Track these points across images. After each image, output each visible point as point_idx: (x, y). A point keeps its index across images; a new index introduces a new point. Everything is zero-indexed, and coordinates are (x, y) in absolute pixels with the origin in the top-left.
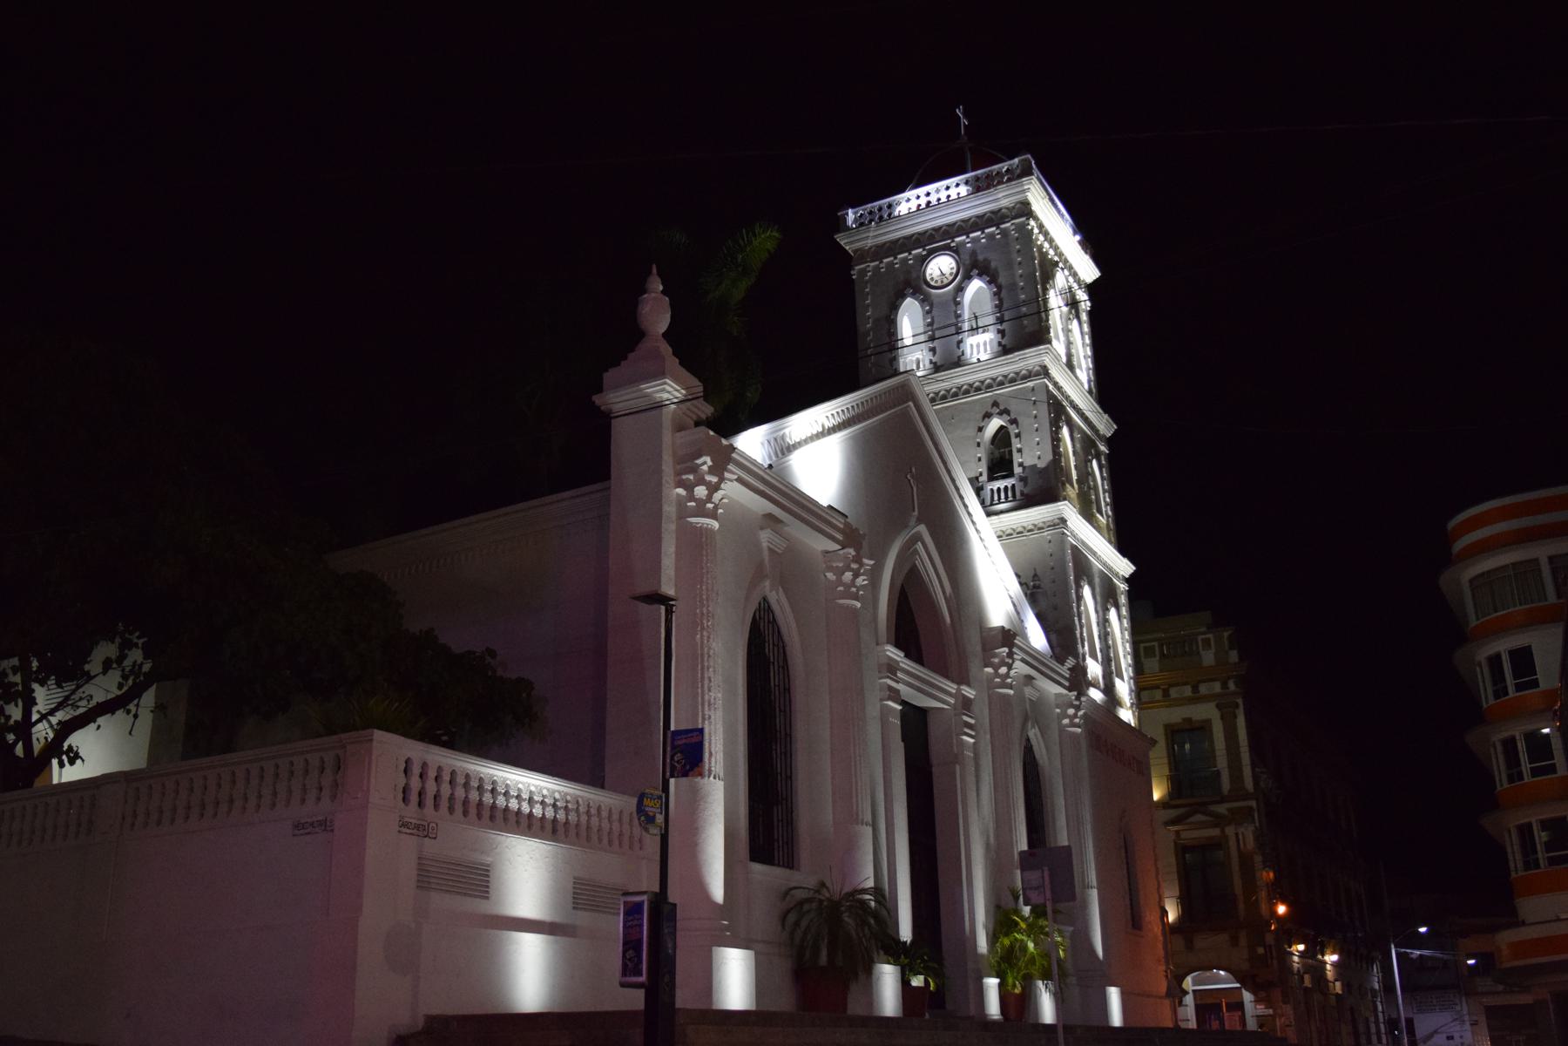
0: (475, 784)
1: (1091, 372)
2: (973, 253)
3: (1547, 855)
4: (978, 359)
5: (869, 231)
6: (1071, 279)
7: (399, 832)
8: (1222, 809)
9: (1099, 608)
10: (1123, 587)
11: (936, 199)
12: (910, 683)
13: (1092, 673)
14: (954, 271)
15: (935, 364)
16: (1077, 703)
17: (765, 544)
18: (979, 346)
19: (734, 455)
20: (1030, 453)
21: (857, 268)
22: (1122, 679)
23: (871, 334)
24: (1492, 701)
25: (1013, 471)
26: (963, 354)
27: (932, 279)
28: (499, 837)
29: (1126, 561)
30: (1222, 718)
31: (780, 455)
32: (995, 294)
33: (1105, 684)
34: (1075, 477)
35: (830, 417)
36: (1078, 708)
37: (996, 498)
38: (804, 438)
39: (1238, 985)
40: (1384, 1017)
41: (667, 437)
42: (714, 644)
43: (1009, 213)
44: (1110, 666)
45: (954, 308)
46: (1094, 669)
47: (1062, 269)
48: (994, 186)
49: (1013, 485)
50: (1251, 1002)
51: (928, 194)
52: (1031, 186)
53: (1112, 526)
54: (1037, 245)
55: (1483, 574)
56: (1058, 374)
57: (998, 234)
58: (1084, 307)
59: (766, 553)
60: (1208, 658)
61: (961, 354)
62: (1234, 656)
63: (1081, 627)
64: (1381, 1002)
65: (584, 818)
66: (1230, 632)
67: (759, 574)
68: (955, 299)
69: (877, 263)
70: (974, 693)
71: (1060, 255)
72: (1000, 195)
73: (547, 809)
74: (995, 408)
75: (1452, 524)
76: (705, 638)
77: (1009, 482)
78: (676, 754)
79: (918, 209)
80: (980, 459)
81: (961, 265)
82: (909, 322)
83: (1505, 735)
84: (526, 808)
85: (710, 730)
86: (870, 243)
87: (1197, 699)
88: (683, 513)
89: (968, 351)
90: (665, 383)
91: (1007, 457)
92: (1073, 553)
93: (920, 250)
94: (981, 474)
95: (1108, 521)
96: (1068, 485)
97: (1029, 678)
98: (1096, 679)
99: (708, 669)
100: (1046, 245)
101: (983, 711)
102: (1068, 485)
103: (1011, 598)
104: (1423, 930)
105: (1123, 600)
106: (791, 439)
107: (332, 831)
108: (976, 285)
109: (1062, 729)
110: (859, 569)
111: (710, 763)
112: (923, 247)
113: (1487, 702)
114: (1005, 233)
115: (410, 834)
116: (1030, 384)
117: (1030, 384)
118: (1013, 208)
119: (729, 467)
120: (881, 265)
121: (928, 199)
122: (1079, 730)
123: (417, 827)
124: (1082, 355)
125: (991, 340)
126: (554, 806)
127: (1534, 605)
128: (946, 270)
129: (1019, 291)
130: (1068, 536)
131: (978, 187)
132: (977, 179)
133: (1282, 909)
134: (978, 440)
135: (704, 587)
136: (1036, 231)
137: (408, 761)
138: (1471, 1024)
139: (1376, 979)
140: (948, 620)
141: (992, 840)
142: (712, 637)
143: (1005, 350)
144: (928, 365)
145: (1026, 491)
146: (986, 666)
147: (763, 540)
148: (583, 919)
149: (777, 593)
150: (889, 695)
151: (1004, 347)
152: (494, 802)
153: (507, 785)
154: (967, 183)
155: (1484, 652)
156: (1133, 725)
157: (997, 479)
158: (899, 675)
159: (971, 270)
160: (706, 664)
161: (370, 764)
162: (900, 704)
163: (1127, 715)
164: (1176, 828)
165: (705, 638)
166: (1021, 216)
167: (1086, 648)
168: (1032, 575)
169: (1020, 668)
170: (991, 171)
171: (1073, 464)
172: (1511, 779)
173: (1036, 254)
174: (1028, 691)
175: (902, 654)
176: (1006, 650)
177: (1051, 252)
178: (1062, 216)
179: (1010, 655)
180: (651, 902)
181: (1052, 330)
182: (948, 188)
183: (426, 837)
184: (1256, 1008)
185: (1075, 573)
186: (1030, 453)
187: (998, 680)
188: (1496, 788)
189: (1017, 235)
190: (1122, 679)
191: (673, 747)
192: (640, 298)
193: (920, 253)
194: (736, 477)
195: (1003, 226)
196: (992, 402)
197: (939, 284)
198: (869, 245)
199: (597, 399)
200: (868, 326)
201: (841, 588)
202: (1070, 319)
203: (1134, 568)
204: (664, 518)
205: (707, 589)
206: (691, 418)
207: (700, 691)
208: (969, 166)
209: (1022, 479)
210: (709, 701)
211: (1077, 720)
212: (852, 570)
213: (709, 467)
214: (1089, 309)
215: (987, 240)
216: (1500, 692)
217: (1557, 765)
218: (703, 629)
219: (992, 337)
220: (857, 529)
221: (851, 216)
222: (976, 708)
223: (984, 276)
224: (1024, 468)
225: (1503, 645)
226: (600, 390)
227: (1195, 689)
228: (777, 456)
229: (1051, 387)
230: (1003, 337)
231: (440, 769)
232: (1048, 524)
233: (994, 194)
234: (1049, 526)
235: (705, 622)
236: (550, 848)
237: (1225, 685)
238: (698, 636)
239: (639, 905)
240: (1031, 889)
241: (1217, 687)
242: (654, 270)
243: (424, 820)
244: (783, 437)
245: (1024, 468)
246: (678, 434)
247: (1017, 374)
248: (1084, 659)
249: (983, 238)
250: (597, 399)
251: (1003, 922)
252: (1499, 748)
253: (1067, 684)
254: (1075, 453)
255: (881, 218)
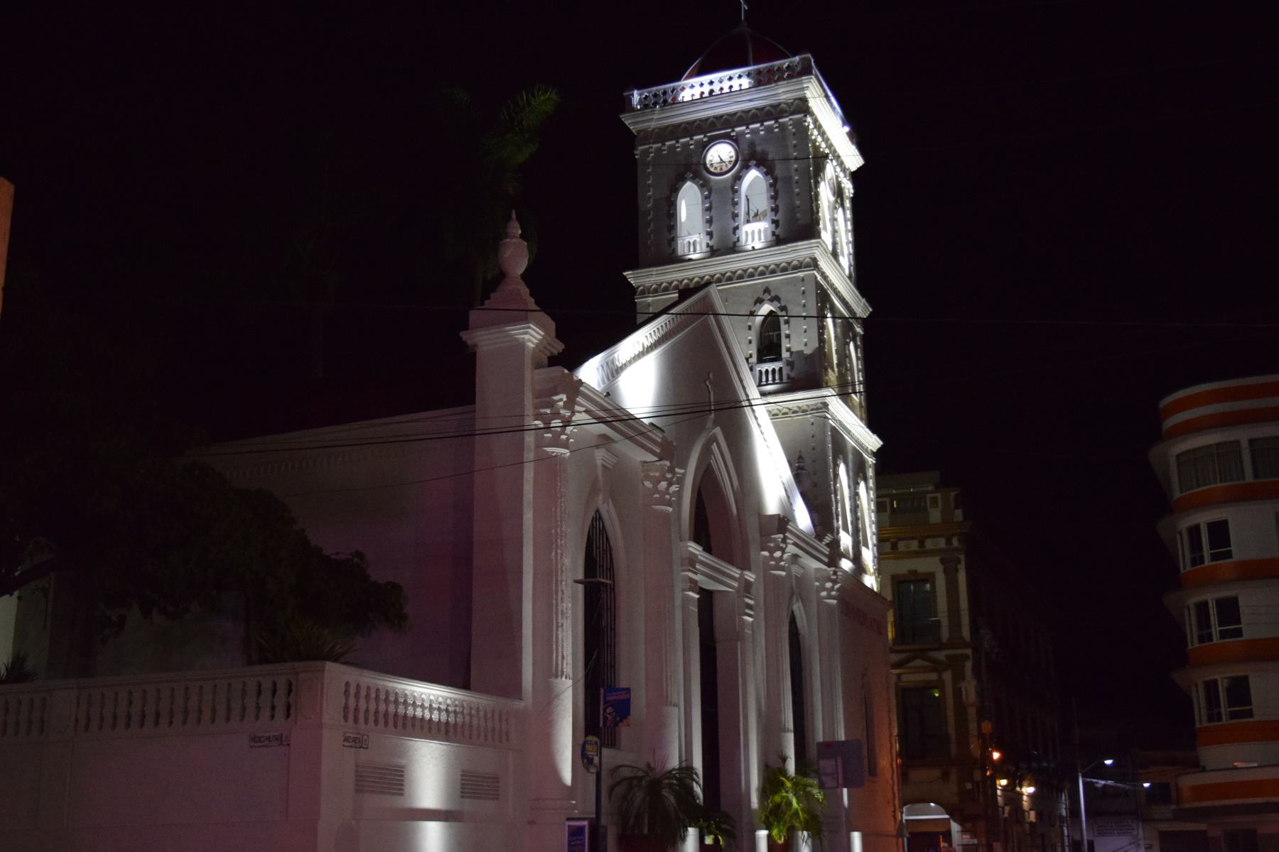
0: (392, 698)
1: (851, 257)
2: (752, 144)
3: (1229, 710)
4: (753, 247)
5: (654, 114)
6: (838, 169)
7: (344, 746)
8: (941, 655)
9: (851, 483)
10: (871, 460)
11: (718, 88)
12: (705, 572)
13: (844, 544)
14: (733, 159)
15: (712, 247)
16: (834, 577)
17: (599, 462)
18: (755, 234)
19: (582, 388)
20: (797, 339)
21: (640, 148)
22: (868, 547)
23: (652, 212)
24: (1189, 568)
25: (780, 355)
26: (738, 240)
27: (712, 165)
28: (408, 741)
29: (875, 437)
30: (945, 571)
31: (611, 378)
32: (771, 185)
33: (854, 554)
34: (835, 361)
35: (649, 335)
36: (835, 582)
37: (764, 379)
38: (628, 359)
39: (947, 816)
40: (1069, 839)
41: (528, 373)
42: (566, 560)
43: (788, 109)
44: (858, 536)
45: (732, 196)
46: (846, 540)
47: (831, 160)
48: (775, 82)
49: (781, 369)
50: (958, 832)
51: (711, 83)
52: (810, 85)
53: (863, 404)
54: (812, 139)
55: (1189, 451)
56: (825, 264)
57: (776, 128)
58: (847, 194)
59: (600, 471)
60: (935, 515)
61: (736, 240)
62: (959, 515)
63: (837, 503)
64: (1067, 827)
65: (467, 718)
66: (955, 493)
67: (594, 491)
68: (732, 187)
69: (659, 145)
70: (754, 577)
71: (830, 146)
72: (781, 91)
73: (442, 714)
74: (766, 294)
75: (1165, 402)
76: (559, 555)
77: (776, 365)
78: (608, 707)
79: (702, 97)
80: (750, 342)
81: (740, 154)
82: (689, 204)
83: (1201, 598)
84: (427, 715)
85: (563, 636)
86: (653, 125)
87: (922, 553)
88: (539, 444)
89: (743, 238)
90: (529, 328)
91: (775, 340)
92: (833, 436)
93: (702, 136)
94: (751, 356)
95: (860, 399)
96: (829, 370)
97: (795, 556)
98: (847, 550)
99: (561, 582)
100: (819, 139)
101: (759, 590)
102: (829, 370)
103: (783, 484)
104: (1108, 762)
105: (870, 473)
106: (619, 361)
107: (289, 745)
108: (753, 174)
109: (820, 600)
110: (672, 478)
111: (562, 665)
112: (704, 133)
113: (1185, 568)
114: (783, 127)
115: (351, 746)
116: (801, 275)
117: (801, 275)
118: (792, 103)
119: (578, 399)
120: (663, 148)
121: (711, 87)
122: (835, 602)
123: (355, 740)
124: (844, 241)
125: (765, 230)
126: (447, 710)
127: (1233, 483)
128: (726, 158)
129: (794, 185)
130: (829, 419)
131: (760, 80)
132: (759, 72)
133: (996, 755)
134: (750, 324)
135: (558, 510)
136: (812, 126)
137: (347, 684)
138: (1146, 848)
139: (1064, 806)
140: (735, 511)
141: (763, 709)
142: (564, 554)
143: (778, 240)
144: (705, 248)
145: (792, 375)
146: (763, 550)
147: (598, 458)
148: (468, 805)
149: (608, 505)
150: (690, 586)
151: (777, 236)
152: (406, 712)
153: (414, 697)
154: (749, 75)
155: (1185, 523)
156: (875, 590)
157: (765, 361)
158: (698, 566)
159: (749, 160)
160: (559, 578)
161: (322, 688)
162: (698, 593)
163: (870, 581)
164: (897, 671)
165: (559, 555)
166: (799, 112)
167: (840, 522)
168: (797, 456)
169: (791, 549)
170: (773, 66)
171: (834, 349)
172: (1202, 640)
173: (811, 149)
174: (794, 569)
175: (700, 549)
176: (782, 536)
177: (823, 145)
178: (833, 108)
179: (784, 540)
180: (591, 826)
181: (821, 222)
182: (730, 79)
183: (360, 748)
184: (962, 838)
185: (833, 452)
186: (797, 339)
187: (773, 563)
188: (1187, 646)
189: (794, 130)
190: (868, 547)
191: (605, 702)
192: (501, 242)
193: (702, 139)
194: (584, 409)
195: (781, 120)
196: (764, 288)
197: (718, 171)
198: (652, 127)
199: (464, 335)
200: (648, 205)
201: (657, 496)
202: (836, 208)
203: (881, 443)
204: (525, 449)
205: (561, 513)
206: (546, 355)
207: (554, 601)
208: (752, 63)
209: (790, 364)
210: (562, 611)
211: (834, 593)
212: (666, 479)
213: (564, 402)
214: (851, 196)
215: (765, 133)
216: (1196, 560)
217: (1243, 629)
218: (557, 545)
219: (767, 226)
220: (671, 442)
221: (636, 97)
222: (753, 590)
223: (761, 167)
224: (792, 353)
225: (1203, 518)
226: (466, 327)
227: (922, 544)
228: (609, 380)
229: (819, 278)
230: (777, 227)
231: (369, 688)
232: (813, 407)
233: (776, 89)
234: (812, 410)
235: (559, 540)
236: (441, 746)
237: (949, 541)
238: (553, 554)
239: (581, 829)
240: (826, 774)
241: (941, 543)
242: (514, 216)
243: (359, 734)
244: (613, 362)
245: (792, 353)
246: (537, 371)
247: (789, 263)
248: (838, 533)
249: (762, 130)
250: (464, 335)
251: (772, 778)
252: (1193, 612)
253: (826, 560)
254: (836, 337)
255: (665, 102)
